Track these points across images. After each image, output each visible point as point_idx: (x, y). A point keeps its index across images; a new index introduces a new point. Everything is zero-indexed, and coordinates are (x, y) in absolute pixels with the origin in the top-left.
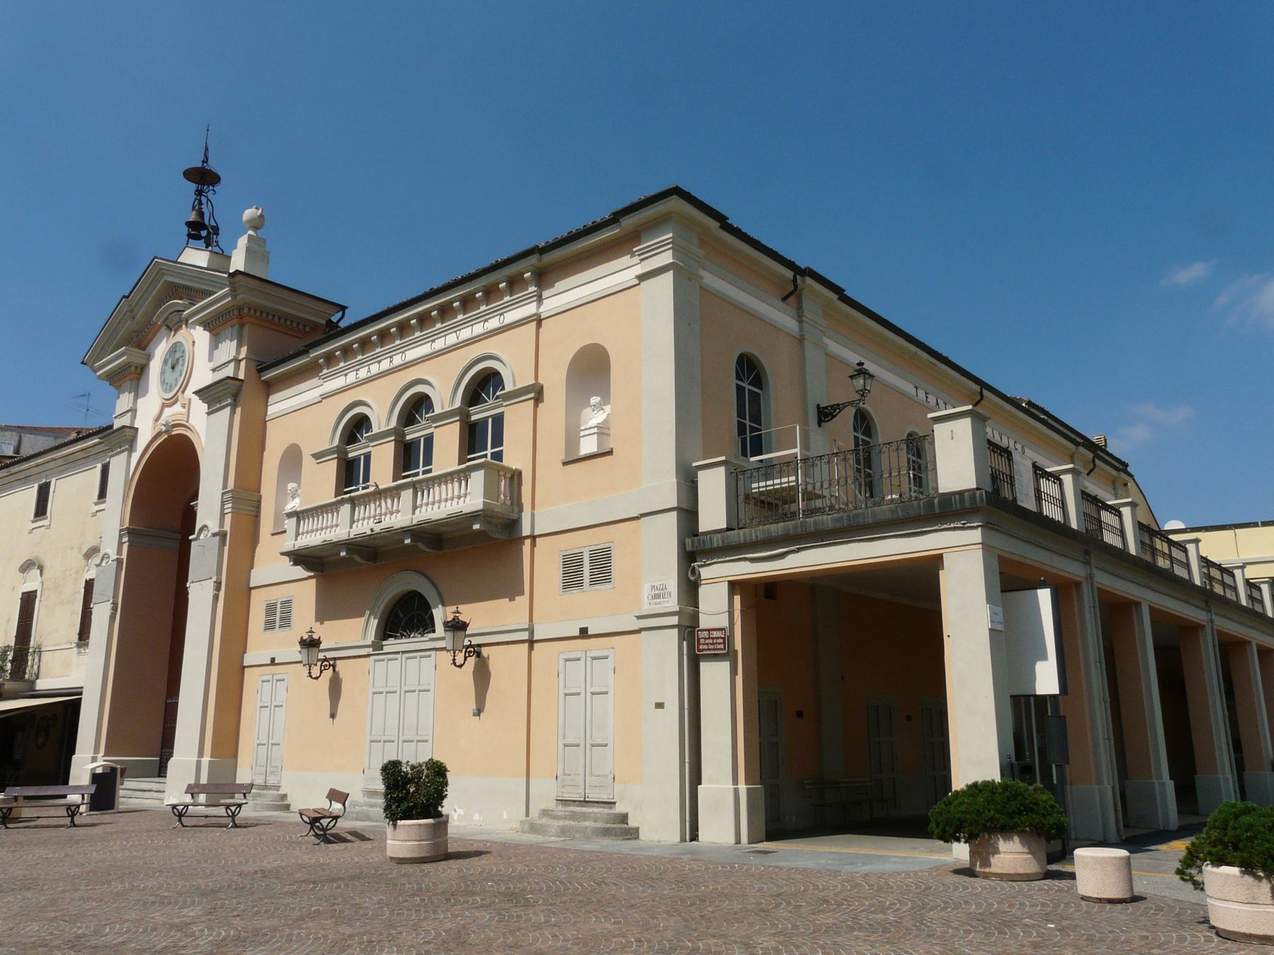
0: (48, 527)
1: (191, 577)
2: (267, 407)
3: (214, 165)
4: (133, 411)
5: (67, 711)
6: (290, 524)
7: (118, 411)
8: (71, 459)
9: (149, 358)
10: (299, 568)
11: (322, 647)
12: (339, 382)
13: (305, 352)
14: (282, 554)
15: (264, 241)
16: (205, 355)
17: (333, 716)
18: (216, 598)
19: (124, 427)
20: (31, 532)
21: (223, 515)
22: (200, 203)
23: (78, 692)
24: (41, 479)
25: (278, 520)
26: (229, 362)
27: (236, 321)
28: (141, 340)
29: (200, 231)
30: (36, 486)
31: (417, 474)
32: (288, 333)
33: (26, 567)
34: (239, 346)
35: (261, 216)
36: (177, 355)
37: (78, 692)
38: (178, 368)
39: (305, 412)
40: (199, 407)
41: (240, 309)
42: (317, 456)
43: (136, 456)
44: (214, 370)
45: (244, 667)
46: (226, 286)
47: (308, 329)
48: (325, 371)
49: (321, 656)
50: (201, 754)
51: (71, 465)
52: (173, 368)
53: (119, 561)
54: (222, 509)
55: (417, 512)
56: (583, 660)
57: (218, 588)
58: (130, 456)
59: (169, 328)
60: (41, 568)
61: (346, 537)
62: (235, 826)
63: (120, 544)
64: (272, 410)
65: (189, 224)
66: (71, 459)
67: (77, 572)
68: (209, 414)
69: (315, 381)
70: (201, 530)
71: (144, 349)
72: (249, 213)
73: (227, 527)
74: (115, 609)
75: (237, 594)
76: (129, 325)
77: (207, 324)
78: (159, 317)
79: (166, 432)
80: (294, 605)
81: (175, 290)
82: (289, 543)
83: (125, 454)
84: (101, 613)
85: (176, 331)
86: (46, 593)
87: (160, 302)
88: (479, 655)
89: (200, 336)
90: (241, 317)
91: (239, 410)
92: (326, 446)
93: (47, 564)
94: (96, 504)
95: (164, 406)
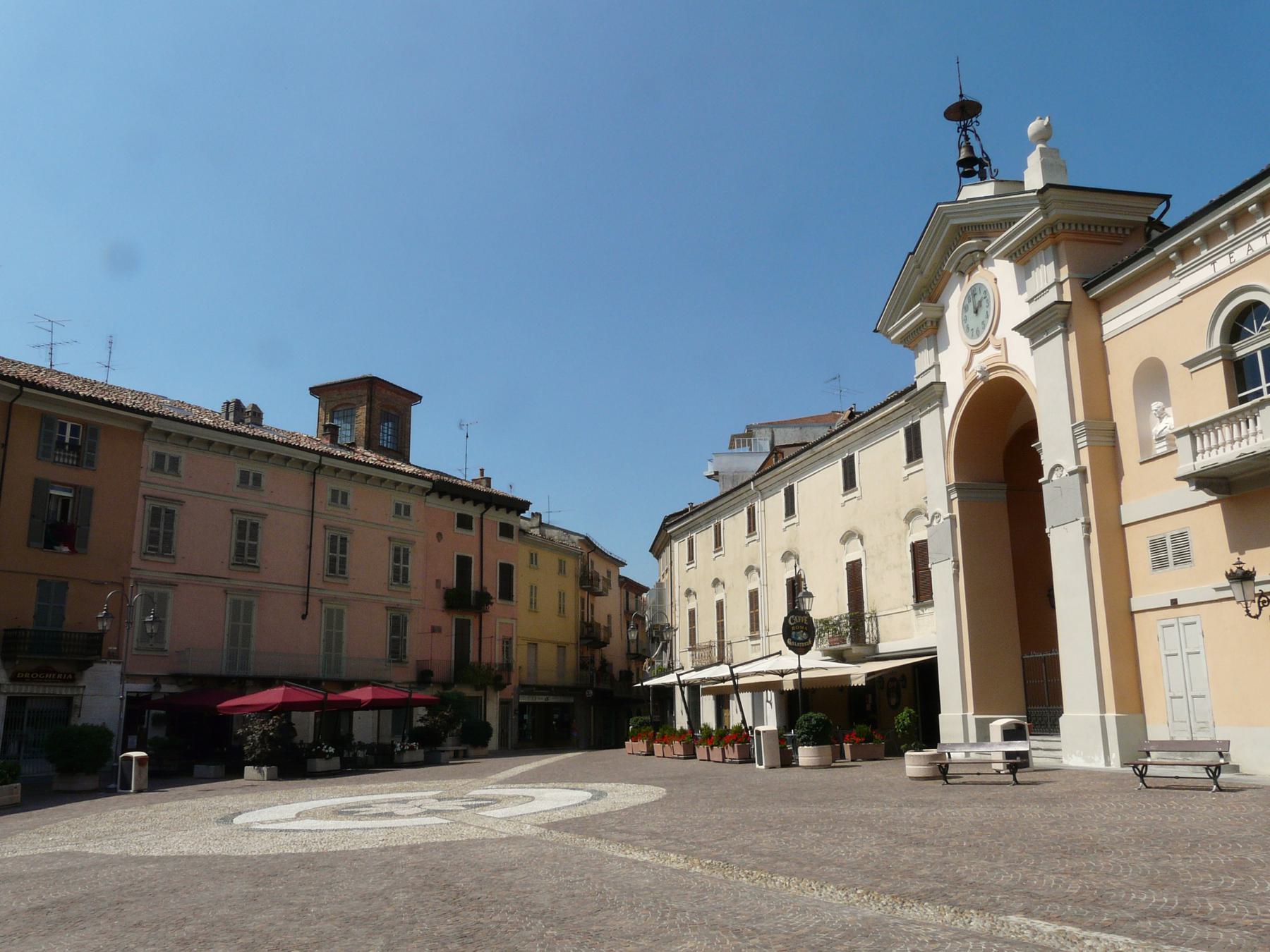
0: (860, 498)
2: (1101, 325)
3: (971, 95)
4: (937, 366)
5: (920, 678)
6: (1184, 443)
8: (871, 428)
9: (943, 309)
10: (1201, 492)
11: (1257, 579)
12: (1206, 273)
14: (1178, 479)
15: (1057, 151)
16: (1012, 290)
18: (1087, 540)
19: (932, 384)
21: (1077, 450)
22: (967, 138)
25: (1145, 443)
26: (1049, 287)
27: (1049, 241)
28: (932, 293)
29: (973, 167)
30: (840, 461)
31: (1260, 393)
32: (1112, 241)
33: (847, 537)
35: (1048, 126)
36: (978, 298)
38: (982, 312)
39: (1169, 317)
40: (1019, 346)
41: (1053, 227)
42: (1190, 364)
43: (949, 412)
44: (1030, 301)
45: (1132, 613)
47: (1127, 232)
48: (1179, 267)
49: (1257, 590)
51: (872, 435)
52: (976, 312)
53: (952, 518)
54: (1076, 444)
55: (1199, 457)
57: (1088, 529)
58: (942, 412)
62: (1220, 789)
63: (950, 501)
64: (1108, 329)
65: (960, 163)
66: (871, 428)
67: (899, 537)
68: (1033, 348)
69: (1166, 282)
70: (1052, 471)
72: (1034, 127)
73: (1085, 461)
74: (957, 567)
75: (1111, 535)
77: (1011, 256)
78: (949, 266)
79: (982, 378)
80: (1191, 537)
81: (962, 232)
82: (1187, 465)
84: (943, 575)
85: (970, 274)
87: (948, 249)
89: (1001, 272)
90: (1054, 235)
91: (1072, 336)
93: (866, 533)
94: (906, 468)
95: (972, 353)
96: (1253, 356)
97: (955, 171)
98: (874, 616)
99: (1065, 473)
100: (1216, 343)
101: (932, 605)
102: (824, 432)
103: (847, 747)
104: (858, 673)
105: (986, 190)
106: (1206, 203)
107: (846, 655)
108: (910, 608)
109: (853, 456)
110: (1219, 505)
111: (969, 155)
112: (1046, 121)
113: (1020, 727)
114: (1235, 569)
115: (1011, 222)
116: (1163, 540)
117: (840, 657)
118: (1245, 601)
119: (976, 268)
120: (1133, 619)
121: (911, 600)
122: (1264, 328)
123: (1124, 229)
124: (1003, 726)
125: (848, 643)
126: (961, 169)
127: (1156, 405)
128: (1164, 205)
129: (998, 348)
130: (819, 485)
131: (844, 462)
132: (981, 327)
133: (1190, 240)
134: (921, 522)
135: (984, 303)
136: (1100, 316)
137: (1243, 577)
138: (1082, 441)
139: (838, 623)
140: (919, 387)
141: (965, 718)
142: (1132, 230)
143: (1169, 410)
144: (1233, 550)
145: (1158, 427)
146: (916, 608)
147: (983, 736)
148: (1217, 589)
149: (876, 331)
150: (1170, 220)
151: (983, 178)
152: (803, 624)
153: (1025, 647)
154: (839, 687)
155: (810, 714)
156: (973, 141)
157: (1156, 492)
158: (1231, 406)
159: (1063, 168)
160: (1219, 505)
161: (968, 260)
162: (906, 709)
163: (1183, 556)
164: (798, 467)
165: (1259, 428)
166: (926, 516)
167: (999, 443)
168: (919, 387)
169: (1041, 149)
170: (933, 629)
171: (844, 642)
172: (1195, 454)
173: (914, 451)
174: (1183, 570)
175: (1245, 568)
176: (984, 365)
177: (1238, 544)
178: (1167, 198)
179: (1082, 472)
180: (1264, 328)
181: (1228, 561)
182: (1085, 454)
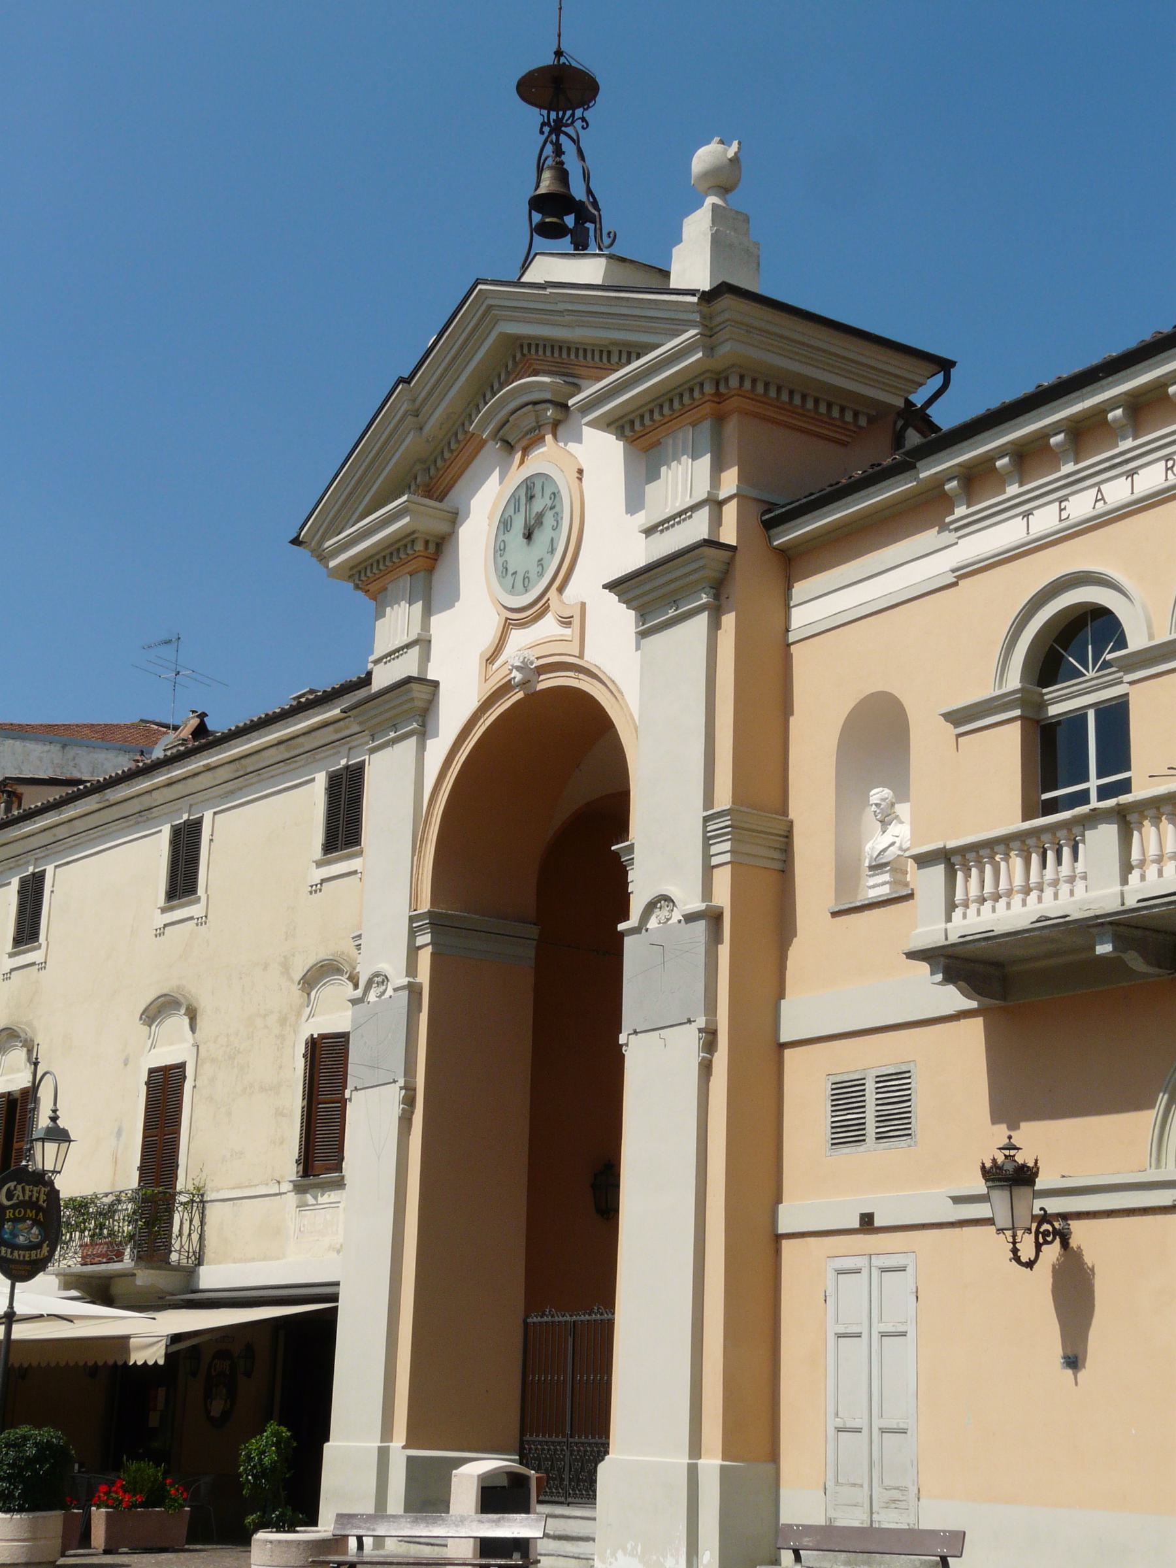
0: (202, 921)
1: (631, 1015)
2: (787, 608)
3: (581, 57)
4: (423, 643)
5: (293, 1351)
7: (381, 646)
9: (455, 518)
10: (951, 989)
11: (1041, 1183)
13: (906, 467)
14: (912, 955)
15: (747, 219)
16: (617, 496)
17: (1073, 1362)
18: (706, 1069)
19: (409, 680)
20: (160, 932)
21: (708, 870)
22: (559, 151)
23: (329, 1294)
24: (179, 812)
25: (846, 872)
26: (693, 508)
27: (707, 408)
28: (436, 478)
29: (563, 216)
30: (166, 830)
32: (833, 434)
33: (158, 1010)
34: (717, 468)
35: (735, 161)
36: (538, 505)
37: (329, 1294)
38: (542, 537)
39: (917, 615)
40: (614, 621)
41: (719, 379)
42: (958, 718)
43: (437, 749)
44: (649, 532)
45: (778, 1238)
46: (692, 324)
47: (863, 422)
48: (961, 511)
50: (695, 1449)
51: (249, 778)
52: (529, 536)
53: (413, 990)
54: (707, 856)
55: (957, 914)
56: (865, 1272)
58: (421, 748)
59: (509, 447)
60: (193, 1015)
61: (1113, 906)
63: (413, 951)
64: (801, 617)
65: (538, 203)
67: (283, 1021)
68: (643, 634)
69: (929, 538)
70: (651, 907)
71: (441, 499)
72: (706, 156)
73: (722, 897)
74: (409, 1101)
75: (755, 1059)
76: (409, 444)
77: (623, 425)
79: (523, 684)
81: (521, 355)
82: (932, 929)
83: (413, 740)
84: (376, 1122)
85: (526, 451)
86: (207, 1069)
87: (486, 386)
88: (1064, 1238)
89: (592, 458)
91: (729, 620)
92: (985, 691)
93: (205, 1004)
95: (508, 626)
96: (1077, 720)
97: (520, 219)
98: (199, 1201)
99: (677, 916)
100: (1013, 681)
101: (340, 1184)
102: (121, 763)
103: (99, 1517)
104: (148, 1335)
105: (589, 270)
106: (1028, 388)
107: (118, 1289)
108: (286, 1187)
109: (198, 823)
110: (979, 1022)
111: (557, 188)
112: (731, 153)
113: (517, 1482)
114: (1000, 1159)
115: (632, 352)
116: (859, 1084)
117: (100, 1291)
118: (1013, 1228)
119: (541, 440)
120: (778, 1252)
121: (290, 1170)
122: (1107, 665)
123: (856, 415)
124: (483, 1478)
125: (127, 1263)
126: (537, 217)
127: (878, 794)
128: (938, 380)
129: (566, 622)
130: (107, 882)
131: (177, 832)
132: (534, 570)
133: (1043, 435)
134: (337, 991)
135: (548, 520)
136: (789, 588)
137: (1012, 1177)
138: (722, 850)
139: (111, 1211)
140: (378, 684)
141: (383, 1455)
142: (871, 420)
143: (903, 809)
144: (995, 1120)
145: (879, 842)
146: (299, 1189)
147: (428, 1494)
148: (957, 1200)
149: (296, 541)
150: (946, 416)
151: (580, 246)
152: (32, 1204)
153: (534, 1299)
154: (101, 1372)
155: (24, 1430)
156: (570, 160)
157: (862, 984)
158: (1025, 818)
159: (753, 258)
160: (979, 1022)
161: (527, 419)
162: (272, 1427)
163: (896, 1122)
164: (62, 832)
165: (1080, 867)
166: (354, 981)
167: (540, 833)
168: (378, 684)
169: (715, 207)
170: (333, 1242)
171: (119, 1256)
172: (951, 906)
173: (343, 829)
174: (893, 1153)
175: (1020, 1159)
176: (531, 655)
177: (1009, 1106)
178: (945, 366)
179: (714, 918)
180: (1107, 665)
181: (988, 1140)
182: (723, 881)
